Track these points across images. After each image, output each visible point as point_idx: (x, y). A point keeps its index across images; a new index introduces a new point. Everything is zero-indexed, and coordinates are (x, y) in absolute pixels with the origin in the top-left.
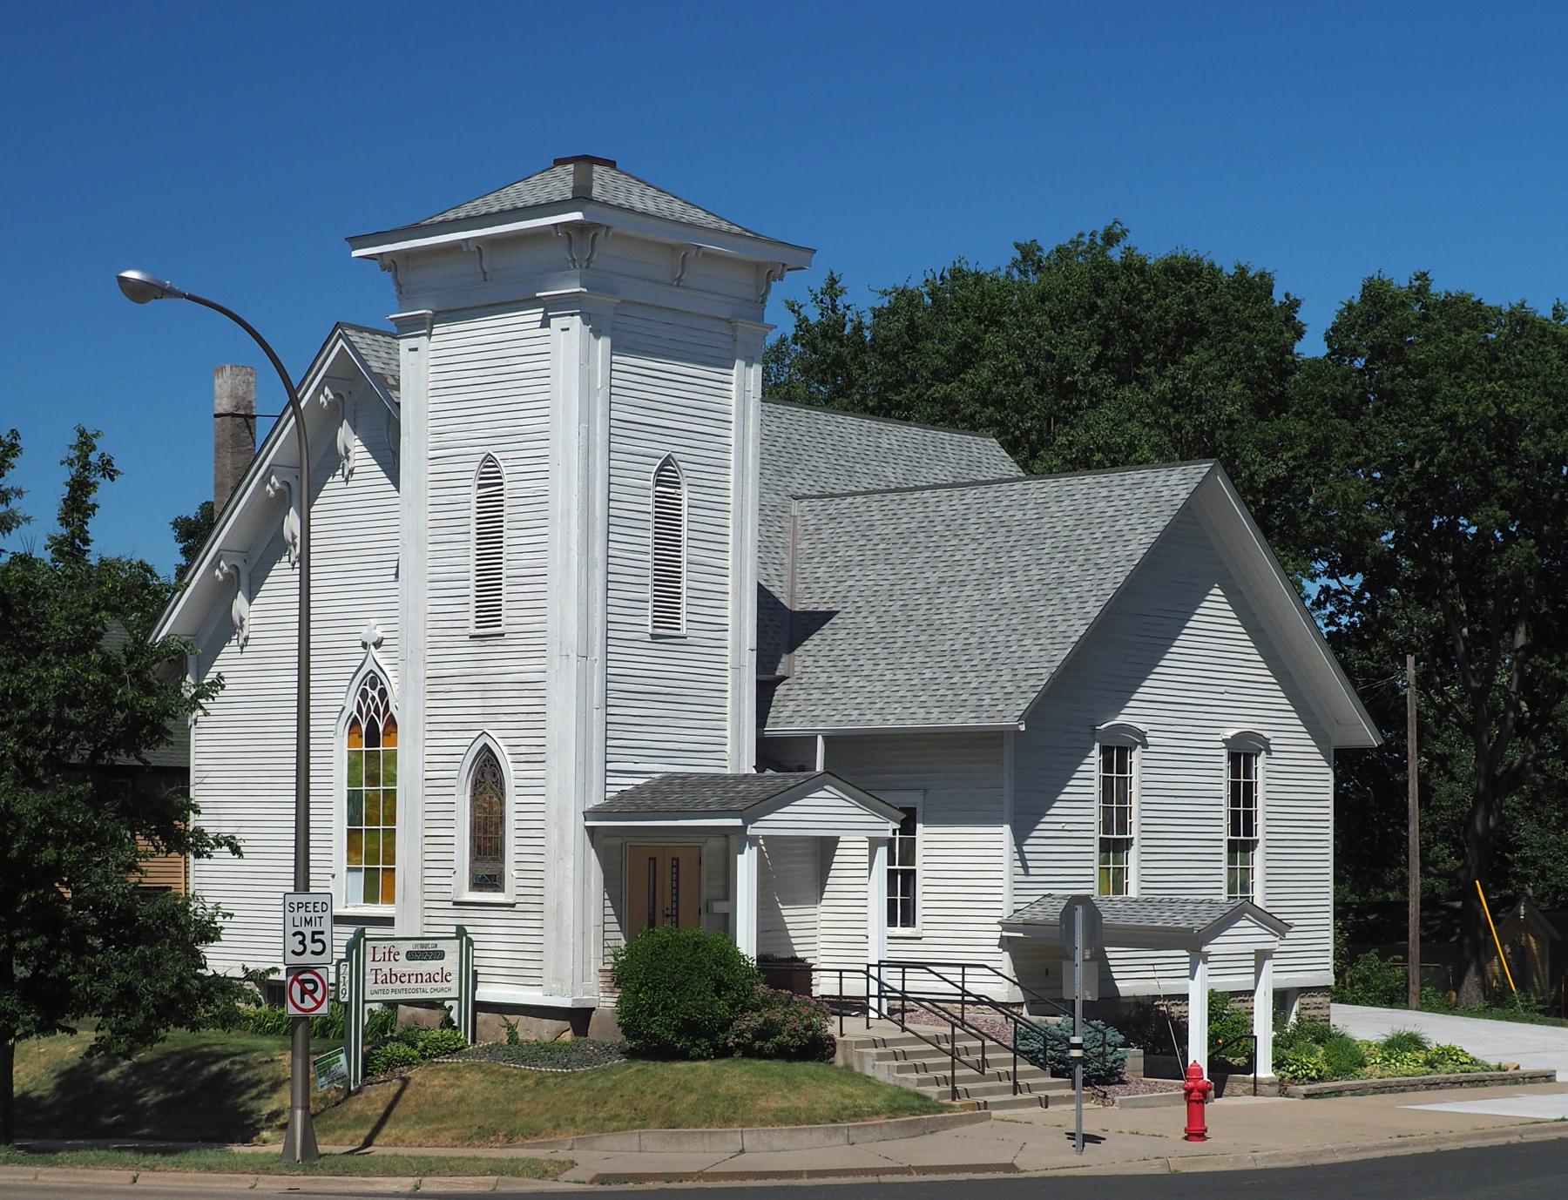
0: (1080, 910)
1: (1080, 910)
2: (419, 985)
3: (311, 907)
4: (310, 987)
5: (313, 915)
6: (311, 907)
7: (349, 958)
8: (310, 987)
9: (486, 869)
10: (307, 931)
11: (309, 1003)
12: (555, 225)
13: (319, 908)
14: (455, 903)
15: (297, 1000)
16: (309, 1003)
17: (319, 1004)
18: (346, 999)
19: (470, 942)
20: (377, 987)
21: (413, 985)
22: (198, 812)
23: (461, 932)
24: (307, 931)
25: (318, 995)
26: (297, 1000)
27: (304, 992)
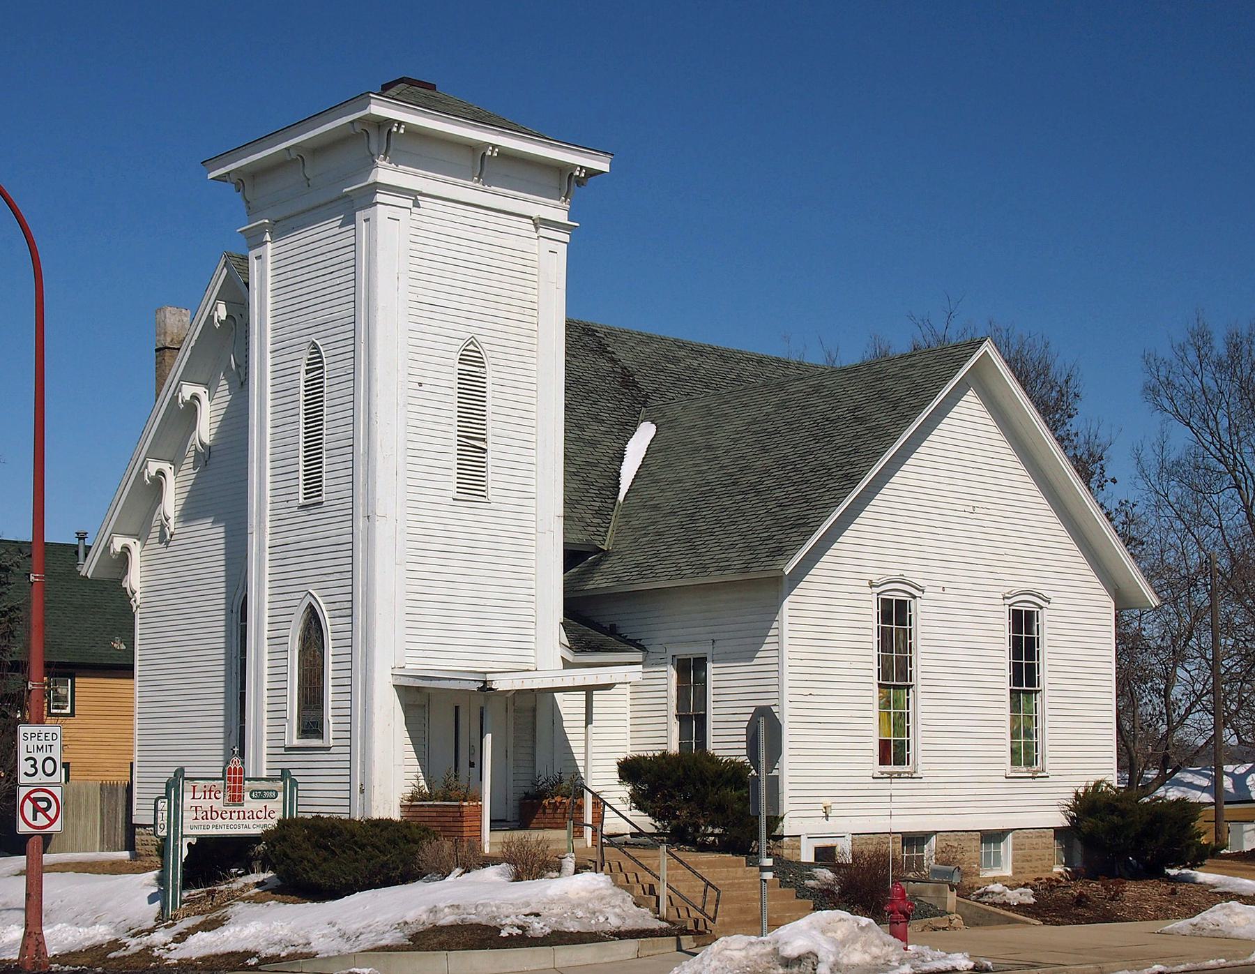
0: (762, 720)
1: (762, 720)
2: (241, 822)
3: (42, 737)
4: (43, 805)
5: (45, 743)
6: (42, 737)
7: (168, 795)
8: (43, 805)
9: (312, 715)
10: (40, 757)
11: (42, 820)
12: (352, 122)
13: (49, 737)
14: (287, 749)
15: (29, 818)
16: (42, 820)
17: (52, 822)
18: (164, 833)
19: (294, 783)
20: (196, 823)
21: (235, 821)
22: (1077, 793)
23: (285, 774)
24: (40, 757)
25: (52, 813)
26: (29, 818)
27: (36, 810)
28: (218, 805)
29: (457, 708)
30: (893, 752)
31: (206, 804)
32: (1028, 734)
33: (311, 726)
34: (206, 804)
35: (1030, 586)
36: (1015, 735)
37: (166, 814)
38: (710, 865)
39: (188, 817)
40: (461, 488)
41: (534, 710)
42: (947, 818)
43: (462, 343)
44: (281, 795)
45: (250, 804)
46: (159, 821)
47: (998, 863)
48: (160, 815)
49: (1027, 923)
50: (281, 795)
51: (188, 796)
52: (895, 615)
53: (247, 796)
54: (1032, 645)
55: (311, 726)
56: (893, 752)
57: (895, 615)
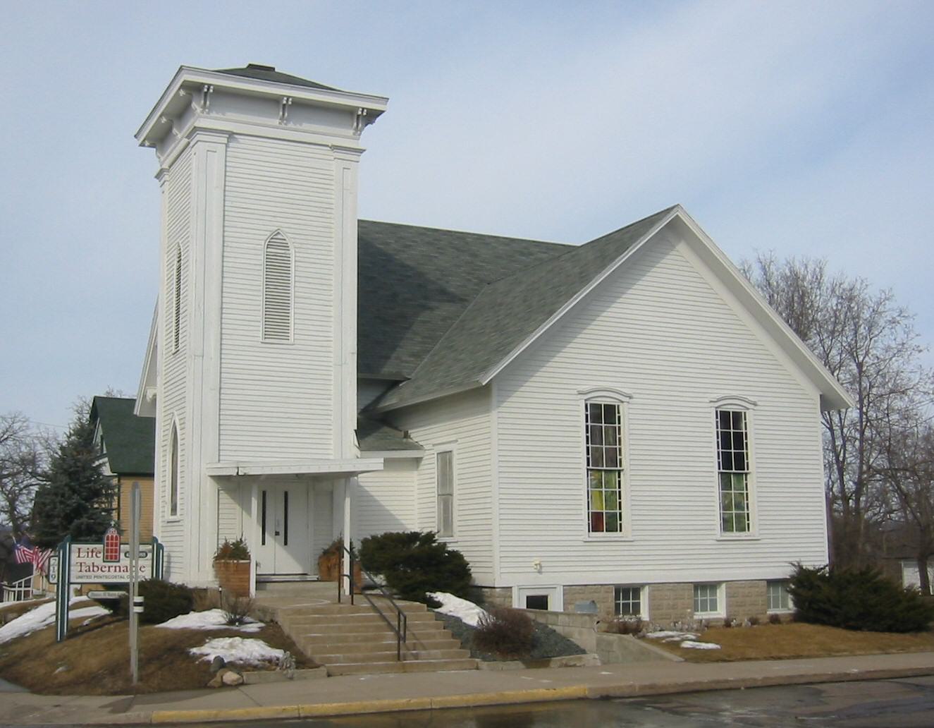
19: (160, 547)
20: (80, 574)
28: (99, 561)
29: (286, 494)
30: (604, 521)
31: (89, 561)
32: (739, 506)
33: (174, 510)
34: (89, 561)
35: (734, 393)
36: (726, 507)
37: (56, 568)
38: (410, 609)
39: (75, 571)
40: (267, 335)
41: (332, 493)
42: (707, 572)
43: (269, 233)
44: (150, 555)
45: (125, 561)
46: (51, 573)
47: (714, 608)
48: (51, 568)
49: (662, 658)
50: (150, 555)
51: (74, 556)
52: (603, 419)
53: (122, 555)
54: (740, 440)
55: (174, 510)
56: (604, 521)
57: (603, 419)
